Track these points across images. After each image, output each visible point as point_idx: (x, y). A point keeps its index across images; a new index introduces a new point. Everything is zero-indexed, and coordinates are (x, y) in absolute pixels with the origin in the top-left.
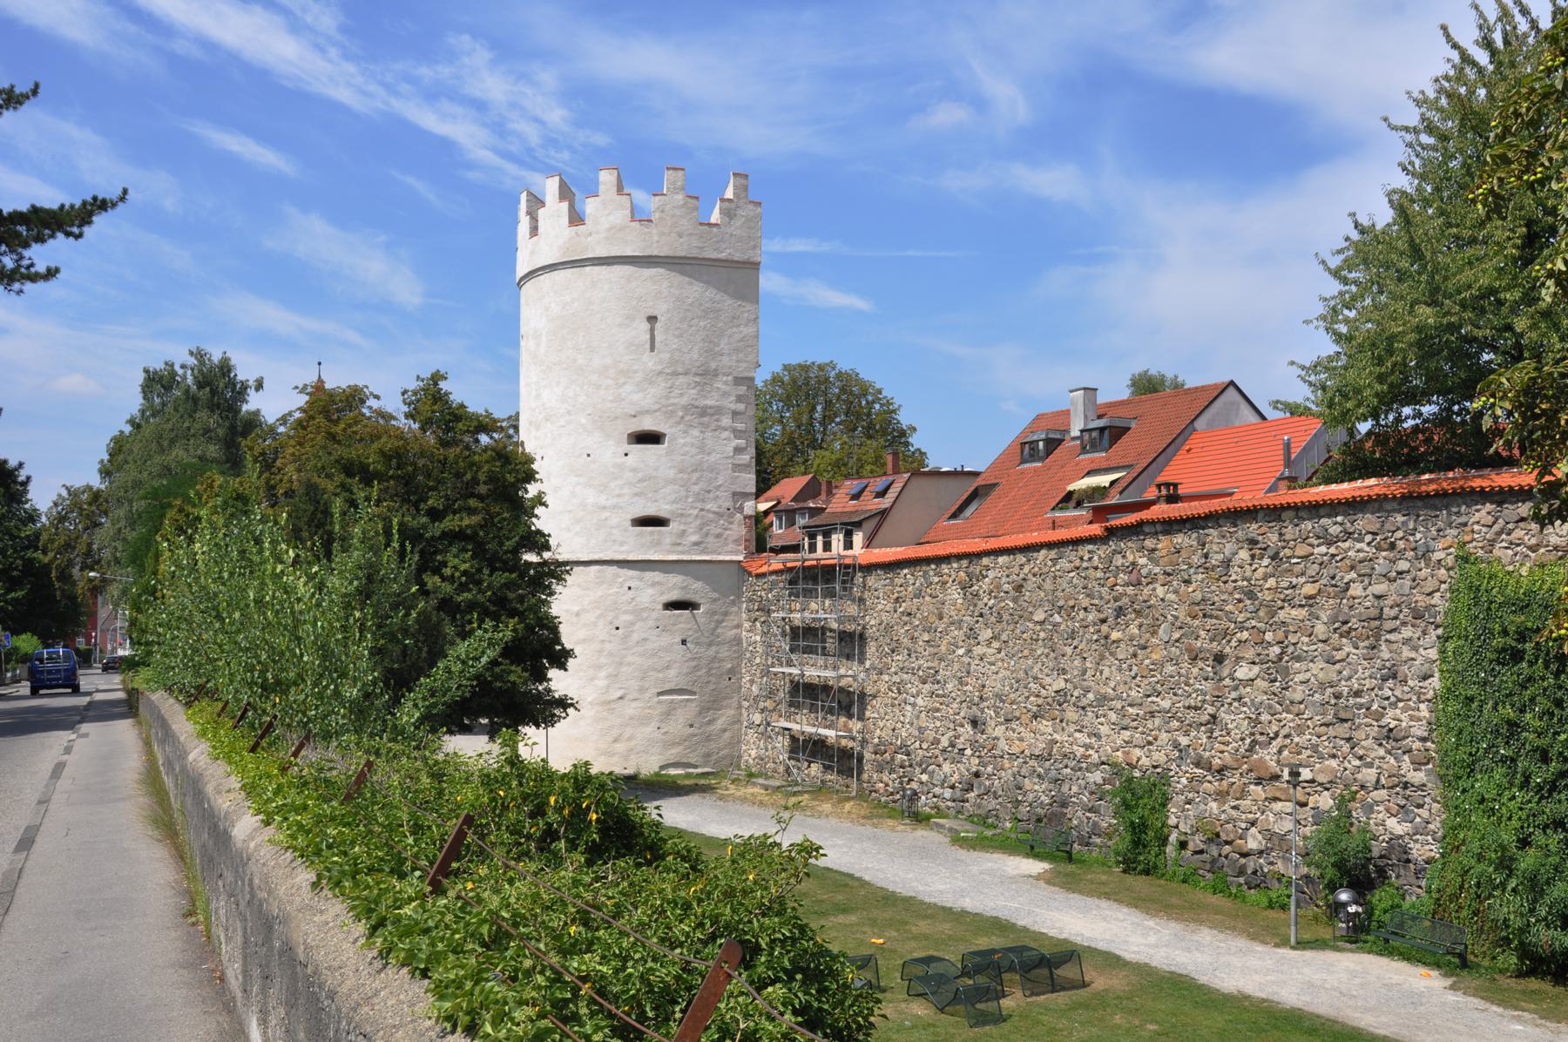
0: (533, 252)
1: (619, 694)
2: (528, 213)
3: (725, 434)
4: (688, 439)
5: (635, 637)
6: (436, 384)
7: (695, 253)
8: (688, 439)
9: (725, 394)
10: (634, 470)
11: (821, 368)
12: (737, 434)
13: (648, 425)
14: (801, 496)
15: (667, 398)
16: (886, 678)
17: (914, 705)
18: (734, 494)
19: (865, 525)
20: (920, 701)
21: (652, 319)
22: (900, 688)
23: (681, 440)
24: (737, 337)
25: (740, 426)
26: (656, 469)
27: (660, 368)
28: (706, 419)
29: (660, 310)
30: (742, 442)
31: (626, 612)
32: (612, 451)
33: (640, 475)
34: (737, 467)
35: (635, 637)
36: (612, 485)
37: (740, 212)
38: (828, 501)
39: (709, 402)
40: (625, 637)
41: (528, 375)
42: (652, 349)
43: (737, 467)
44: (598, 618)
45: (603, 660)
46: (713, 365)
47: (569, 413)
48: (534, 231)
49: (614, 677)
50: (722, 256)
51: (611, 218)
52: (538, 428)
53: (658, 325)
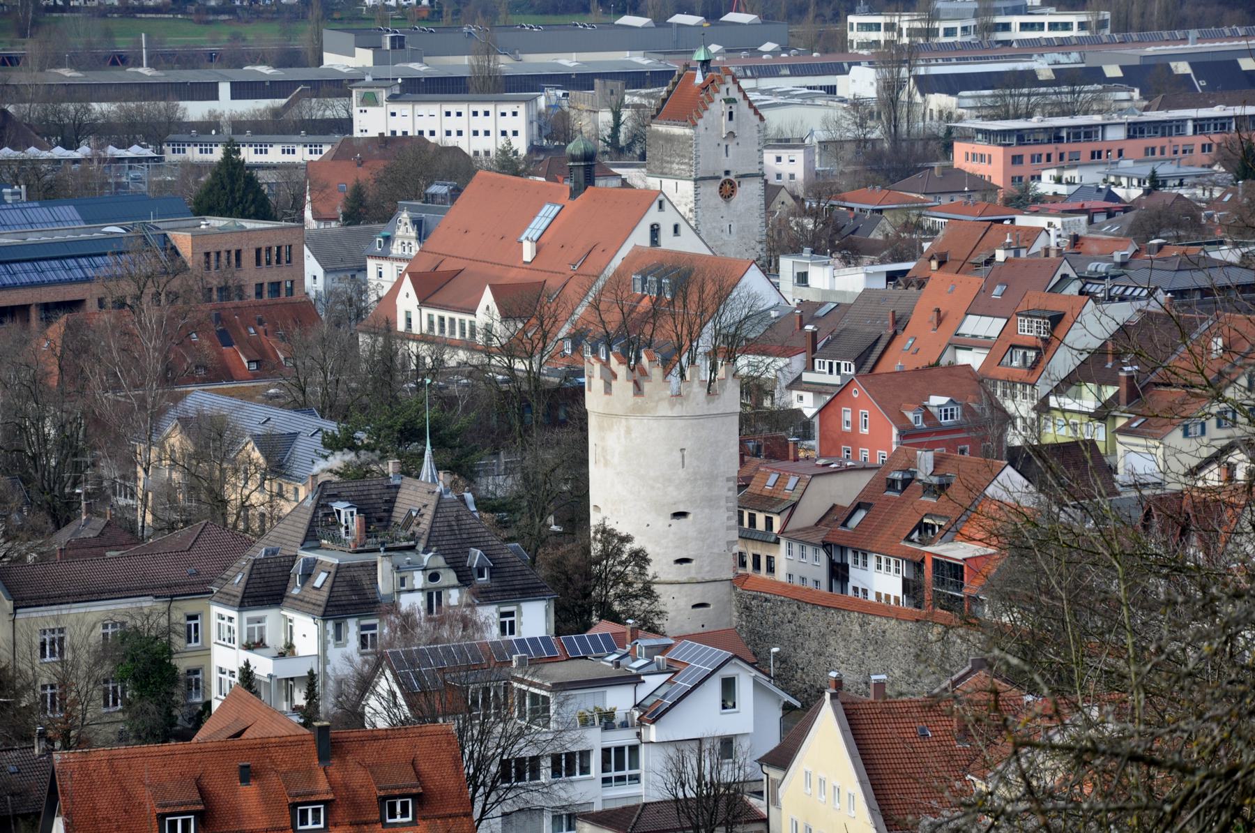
10: (675, 534)
12: (728, 509)
29: (688, 445)
34: (729, 528)
43: (729, 528)
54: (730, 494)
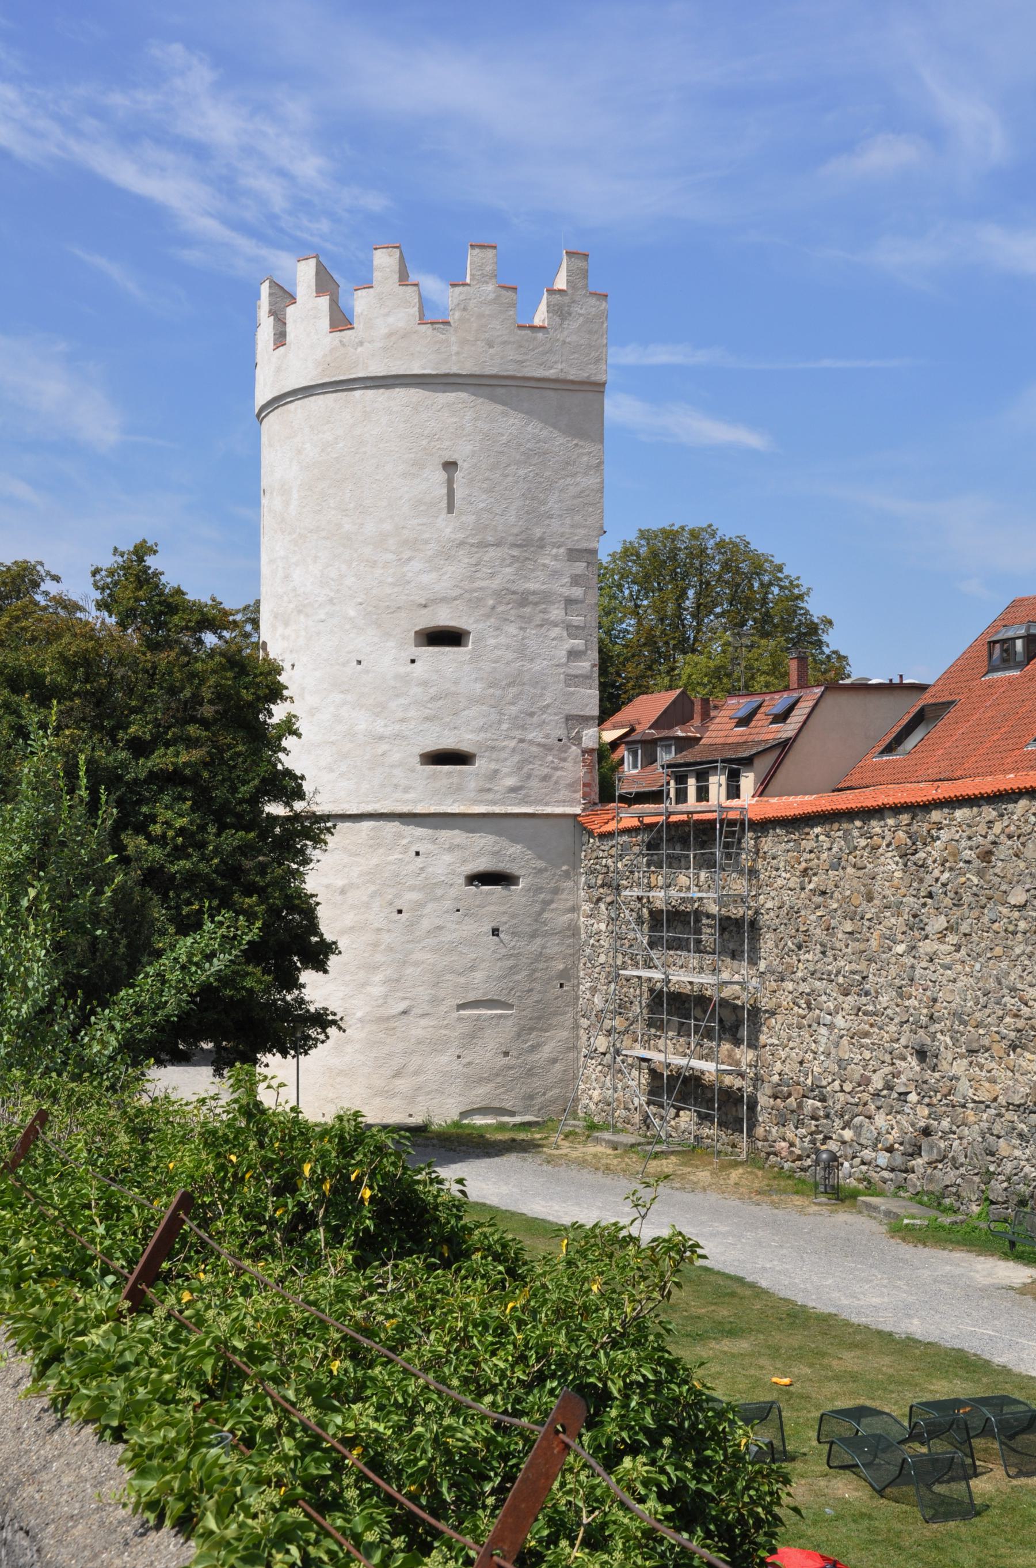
0: (278, 370)
1: (402, 1006)
2: (272, 313)
3: (556, 632)
4: (502, 640)
5: (426, 924)
6: (141, 560)
7: (511, 370)
8: (502, 640)
9: (555, 574)
10: (425, 684)
11: (694, 534)
13: (444, 618)
14: (664, 721)
15: (472, 579)
16: (789, 986)
17: (831, 1027)
18: (568, 718)
19: (757, 763)
20: (839, 1021)
21: (450, 466)
22: (810, 1001)
23: (491, 640)
24: (573, 490)
25: (577, 620)
26: (456, 683)
27: (460, 536)
28: (528, 610)
29: (462, 452)
30: (579, 643)
31: (412, 888)
32: (392, 655)
33: (433, 691)
34: (572, 679)
35: (426, 924)
36: (393, 705)
37: (576, 309)
38: (704, 728)
39: (532, 586)
40: (411, 925)
41: (273, 547)
42: (450, 508)
43: (572, 679)
44: (372, 896)
45: (379, 958)
46: (538, 532)
47: (331, 601)
48: (280, 338)
49: (395, 983)
50: (551, 373)
51: (391, 320)
52: (286, 624)
53: (458, 475)
54: (578, 592)
